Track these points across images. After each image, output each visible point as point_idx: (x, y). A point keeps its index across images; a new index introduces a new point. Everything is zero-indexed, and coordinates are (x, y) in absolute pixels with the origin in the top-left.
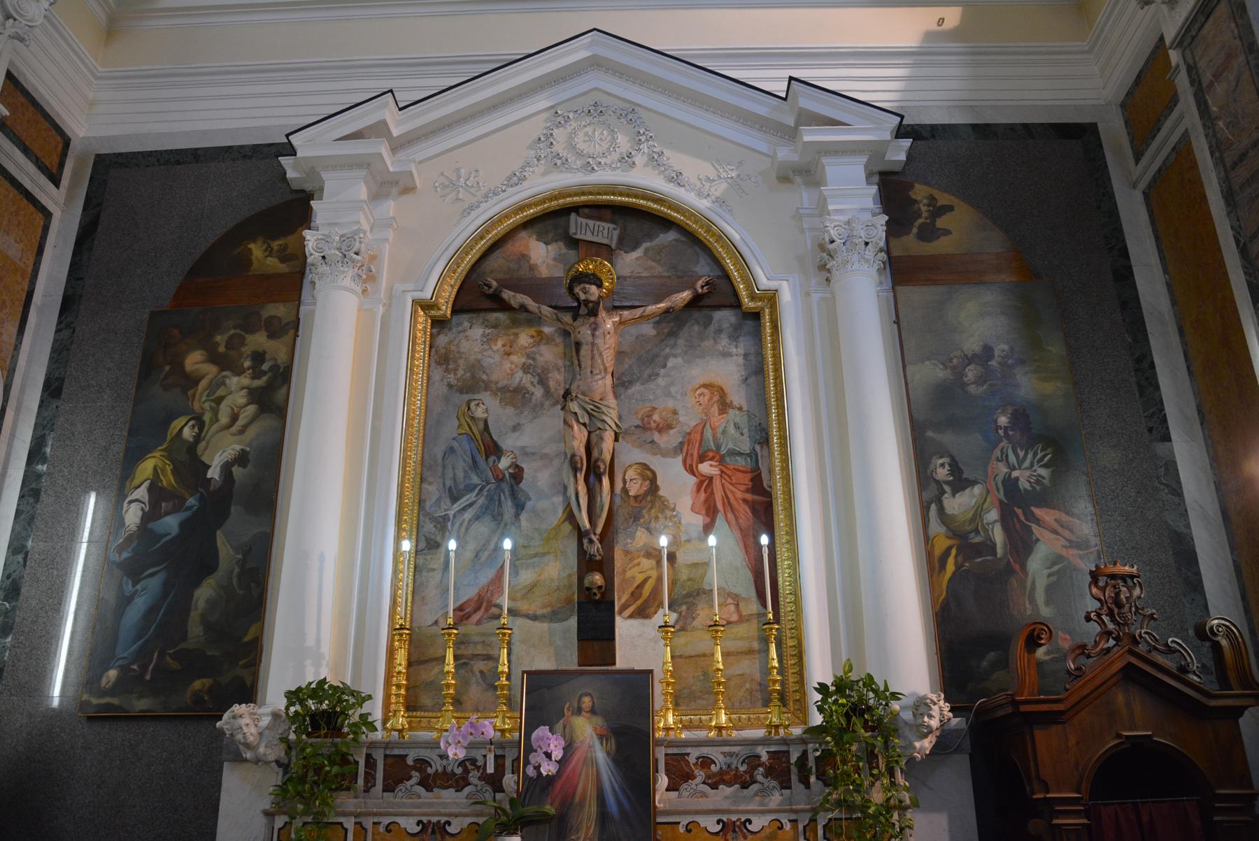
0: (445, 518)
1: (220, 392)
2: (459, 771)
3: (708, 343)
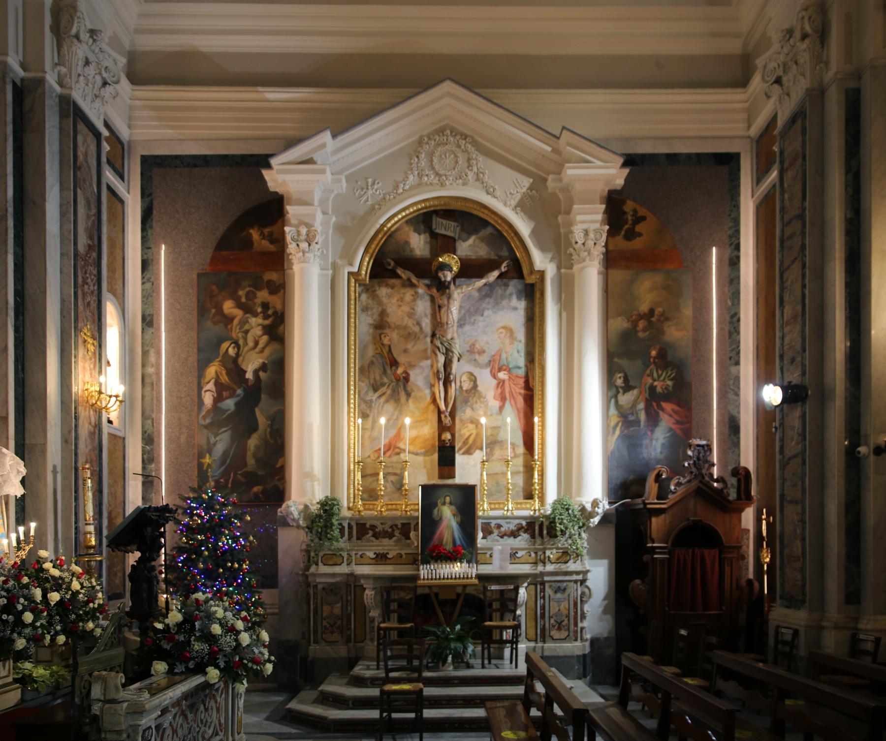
0: (371, 401)
1: (246, 327)
2: (390, 530)
3: (505, 302)
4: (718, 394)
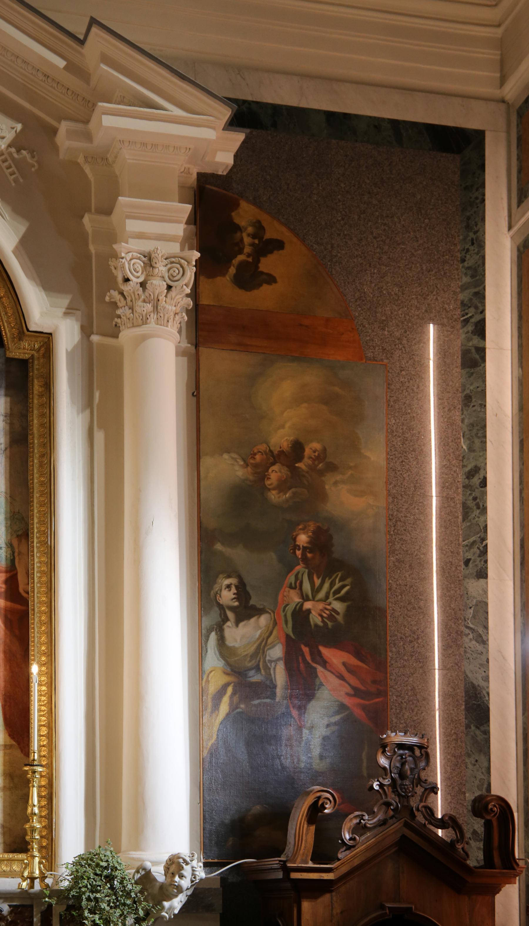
4: (442, 637)
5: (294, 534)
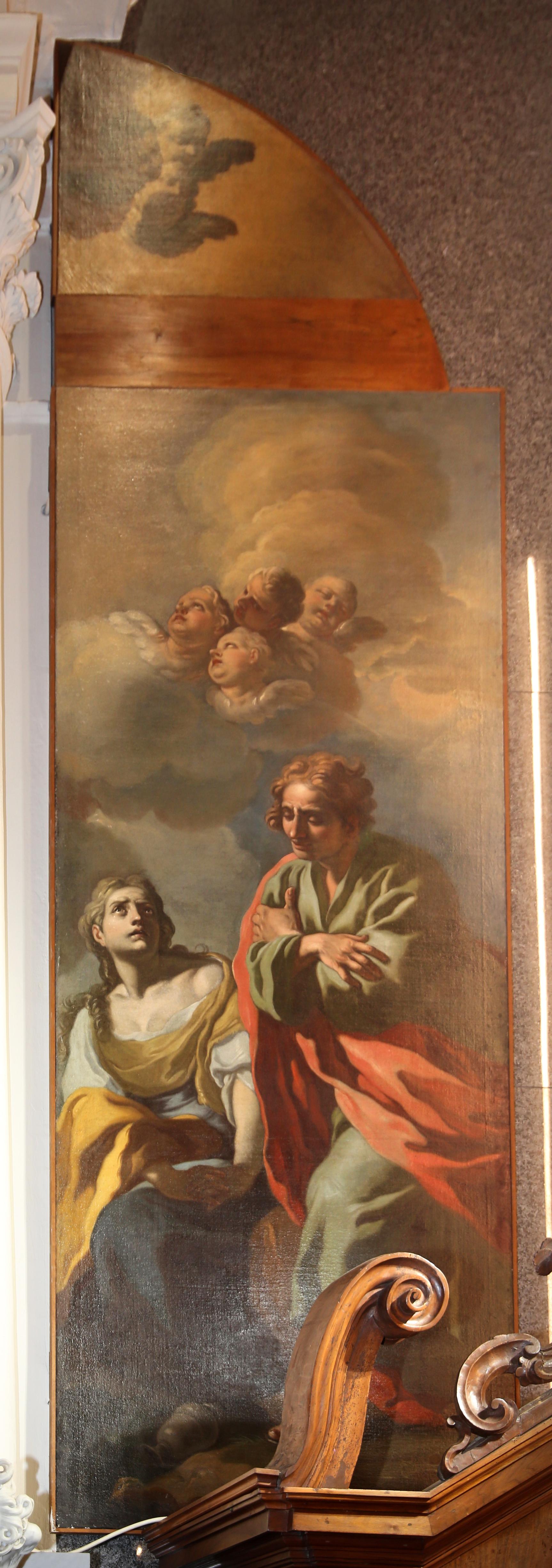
5: (279, 783)
